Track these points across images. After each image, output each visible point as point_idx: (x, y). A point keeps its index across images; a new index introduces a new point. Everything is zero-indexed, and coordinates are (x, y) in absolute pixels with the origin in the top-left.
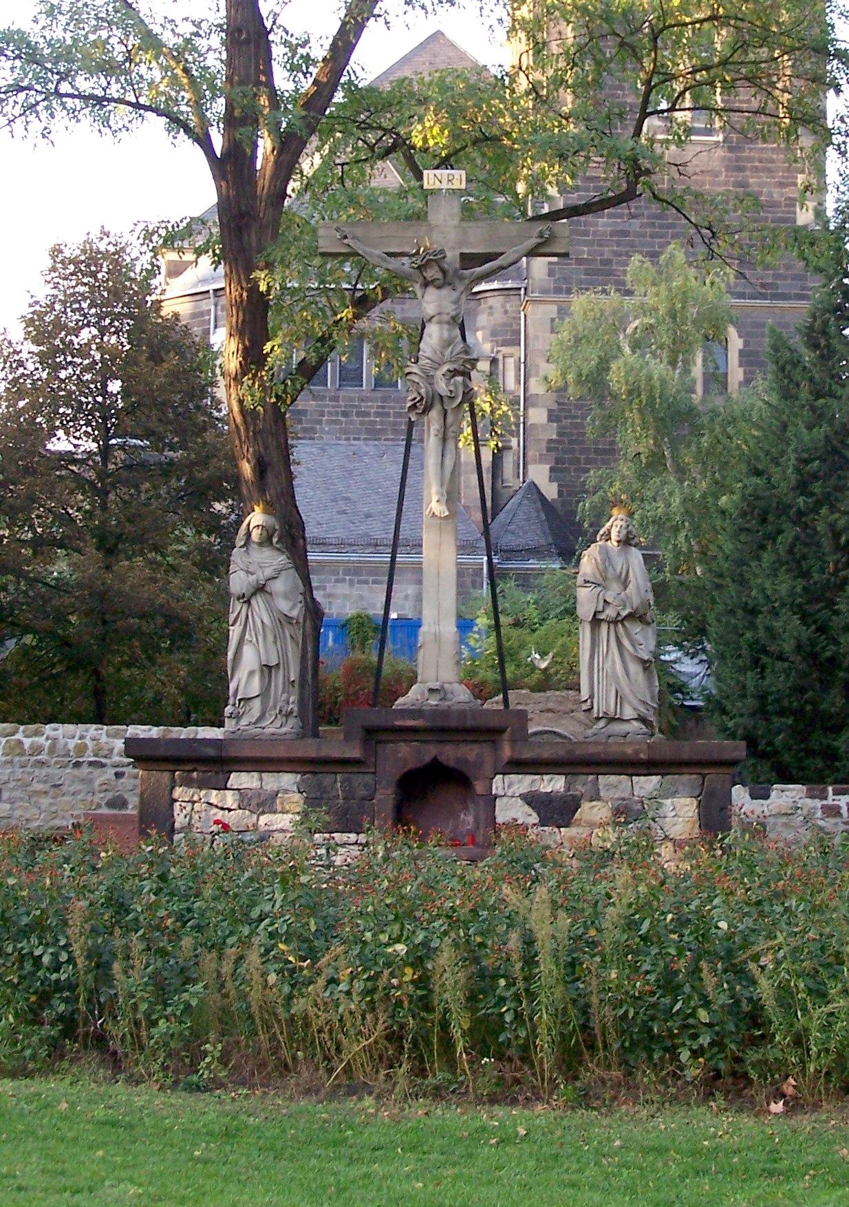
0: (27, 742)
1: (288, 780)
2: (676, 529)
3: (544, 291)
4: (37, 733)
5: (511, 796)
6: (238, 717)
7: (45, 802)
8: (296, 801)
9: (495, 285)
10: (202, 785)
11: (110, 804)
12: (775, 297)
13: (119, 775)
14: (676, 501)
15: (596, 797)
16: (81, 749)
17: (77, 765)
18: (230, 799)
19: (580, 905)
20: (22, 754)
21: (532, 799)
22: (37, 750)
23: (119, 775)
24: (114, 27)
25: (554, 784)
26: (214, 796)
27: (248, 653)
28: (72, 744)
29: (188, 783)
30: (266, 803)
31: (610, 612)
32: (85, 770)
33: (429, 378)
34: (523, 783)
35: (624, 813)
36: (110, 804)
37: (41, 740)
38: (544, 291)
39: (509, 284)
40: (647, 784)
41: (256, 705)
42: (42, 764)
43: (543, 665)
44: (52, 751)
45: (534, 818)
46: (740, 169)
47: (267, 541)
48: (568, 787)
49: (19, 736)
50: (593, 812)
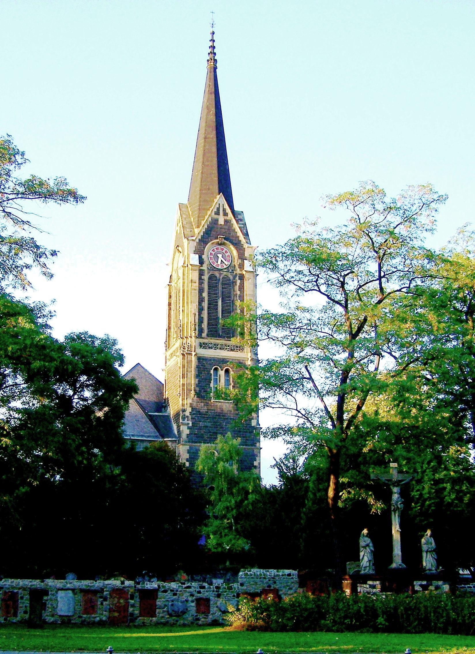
0: (249, 573)
2: (232, 509)
4: (250, 571)
6: (365, 570)
8: (379, 587)
9: (170, 439)
11: (267, 587)
13: (269, 580)
16: (261, 574)
17: (261, 578)
18: (368, 586)
19: (295, 608)
20: (248, 575)
21: (421, 586)
23: (269, 580)
24: (81, 366)
26: (365, 586)
28: (258, 573)
30: (374, 587)
31: (430, 550)
32: (262, 579)
33: (397, 505)
34: (419, 583)
37: (251, 572)
41: (368, 568)
42: (252, 578)
43: (228, 548)
45: (421, 589)
46: (237, 410)
47: (367, 536)
48: (427, 582)
49: (246, 572)
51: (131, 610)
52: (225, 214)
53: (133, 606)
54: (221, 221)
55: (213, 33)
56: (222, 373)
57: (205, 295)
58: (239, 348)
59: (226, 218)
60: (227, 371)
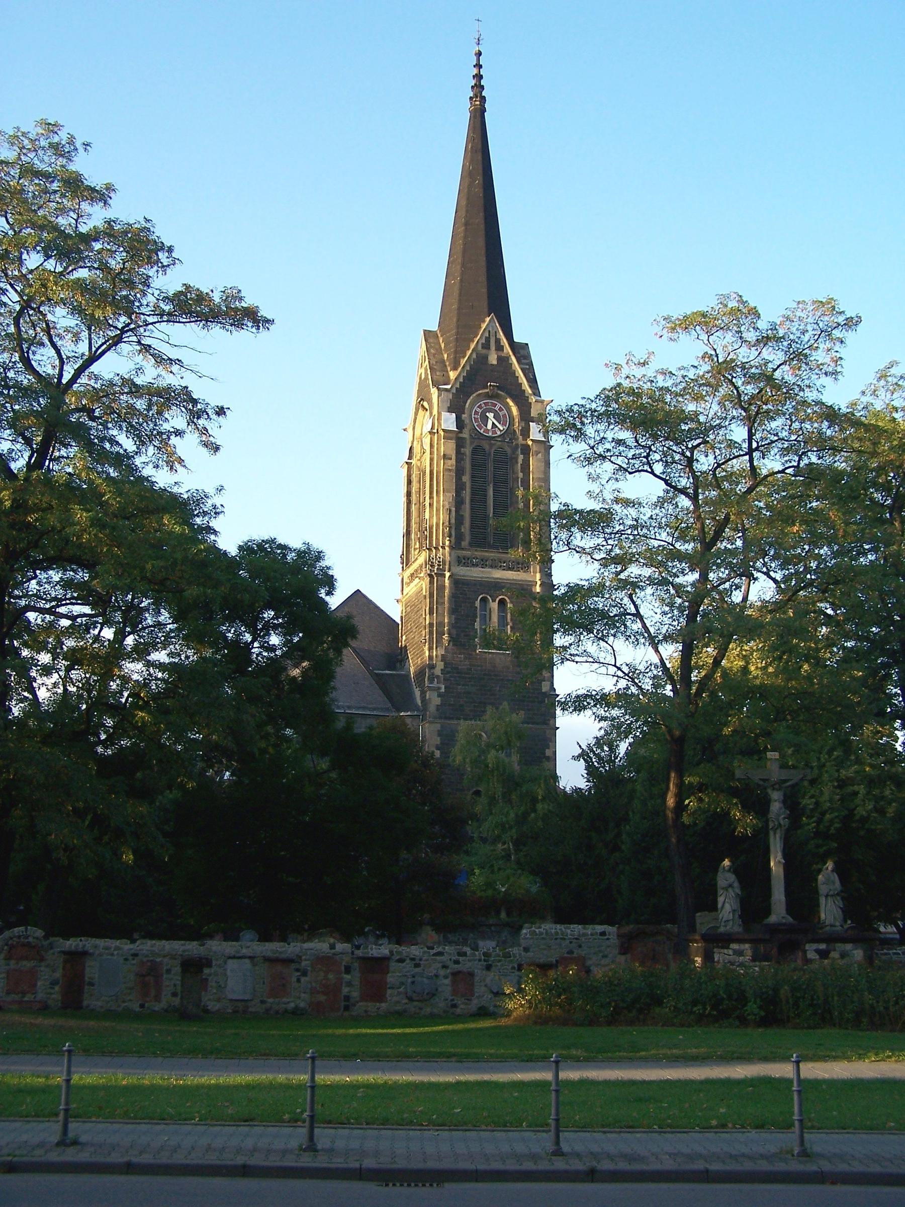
1: (747, 946)
3: (435, 718)
4: (540, 928)
5: (811, 951)
6: (726, 926)
7: (545, 952)
8: (749, 953)
10: (723, 948)
11: (568, 953)
12: (533, 723)
13: (571, 942)
14: (512, 815)
15: (835, 950)
16: (557, 933)
18: (731, 952)
22: (541, 934)
23: (571, 942)
25: (823, 946)
26: (726, 951)
27: (727, 906)
28: (553, 931)
29: (718, 947)
31: (831, 893)
32: (558, 941)
34: (815, 946)
35: (843, 955)
36: (568, 953)
37: (542, 930)
38: (435, 718)
39: (416, 713)
40: (849, 947)
42: (543, 938)
44: (547, 933)
45: (818, 957)
50: (834, 955)
51: (345, 990)
52: (500, 348)
53: (349, 984)
54: (493, 359)
55: (479, 54)
56: (494, 606)
57: (466, 478)
58: (522, 565)
59: (500, 353)
60: (502, 603)
